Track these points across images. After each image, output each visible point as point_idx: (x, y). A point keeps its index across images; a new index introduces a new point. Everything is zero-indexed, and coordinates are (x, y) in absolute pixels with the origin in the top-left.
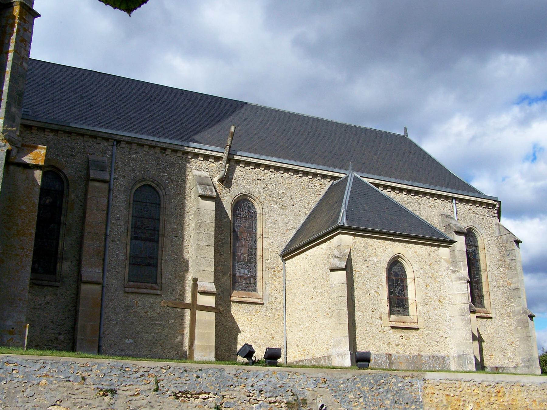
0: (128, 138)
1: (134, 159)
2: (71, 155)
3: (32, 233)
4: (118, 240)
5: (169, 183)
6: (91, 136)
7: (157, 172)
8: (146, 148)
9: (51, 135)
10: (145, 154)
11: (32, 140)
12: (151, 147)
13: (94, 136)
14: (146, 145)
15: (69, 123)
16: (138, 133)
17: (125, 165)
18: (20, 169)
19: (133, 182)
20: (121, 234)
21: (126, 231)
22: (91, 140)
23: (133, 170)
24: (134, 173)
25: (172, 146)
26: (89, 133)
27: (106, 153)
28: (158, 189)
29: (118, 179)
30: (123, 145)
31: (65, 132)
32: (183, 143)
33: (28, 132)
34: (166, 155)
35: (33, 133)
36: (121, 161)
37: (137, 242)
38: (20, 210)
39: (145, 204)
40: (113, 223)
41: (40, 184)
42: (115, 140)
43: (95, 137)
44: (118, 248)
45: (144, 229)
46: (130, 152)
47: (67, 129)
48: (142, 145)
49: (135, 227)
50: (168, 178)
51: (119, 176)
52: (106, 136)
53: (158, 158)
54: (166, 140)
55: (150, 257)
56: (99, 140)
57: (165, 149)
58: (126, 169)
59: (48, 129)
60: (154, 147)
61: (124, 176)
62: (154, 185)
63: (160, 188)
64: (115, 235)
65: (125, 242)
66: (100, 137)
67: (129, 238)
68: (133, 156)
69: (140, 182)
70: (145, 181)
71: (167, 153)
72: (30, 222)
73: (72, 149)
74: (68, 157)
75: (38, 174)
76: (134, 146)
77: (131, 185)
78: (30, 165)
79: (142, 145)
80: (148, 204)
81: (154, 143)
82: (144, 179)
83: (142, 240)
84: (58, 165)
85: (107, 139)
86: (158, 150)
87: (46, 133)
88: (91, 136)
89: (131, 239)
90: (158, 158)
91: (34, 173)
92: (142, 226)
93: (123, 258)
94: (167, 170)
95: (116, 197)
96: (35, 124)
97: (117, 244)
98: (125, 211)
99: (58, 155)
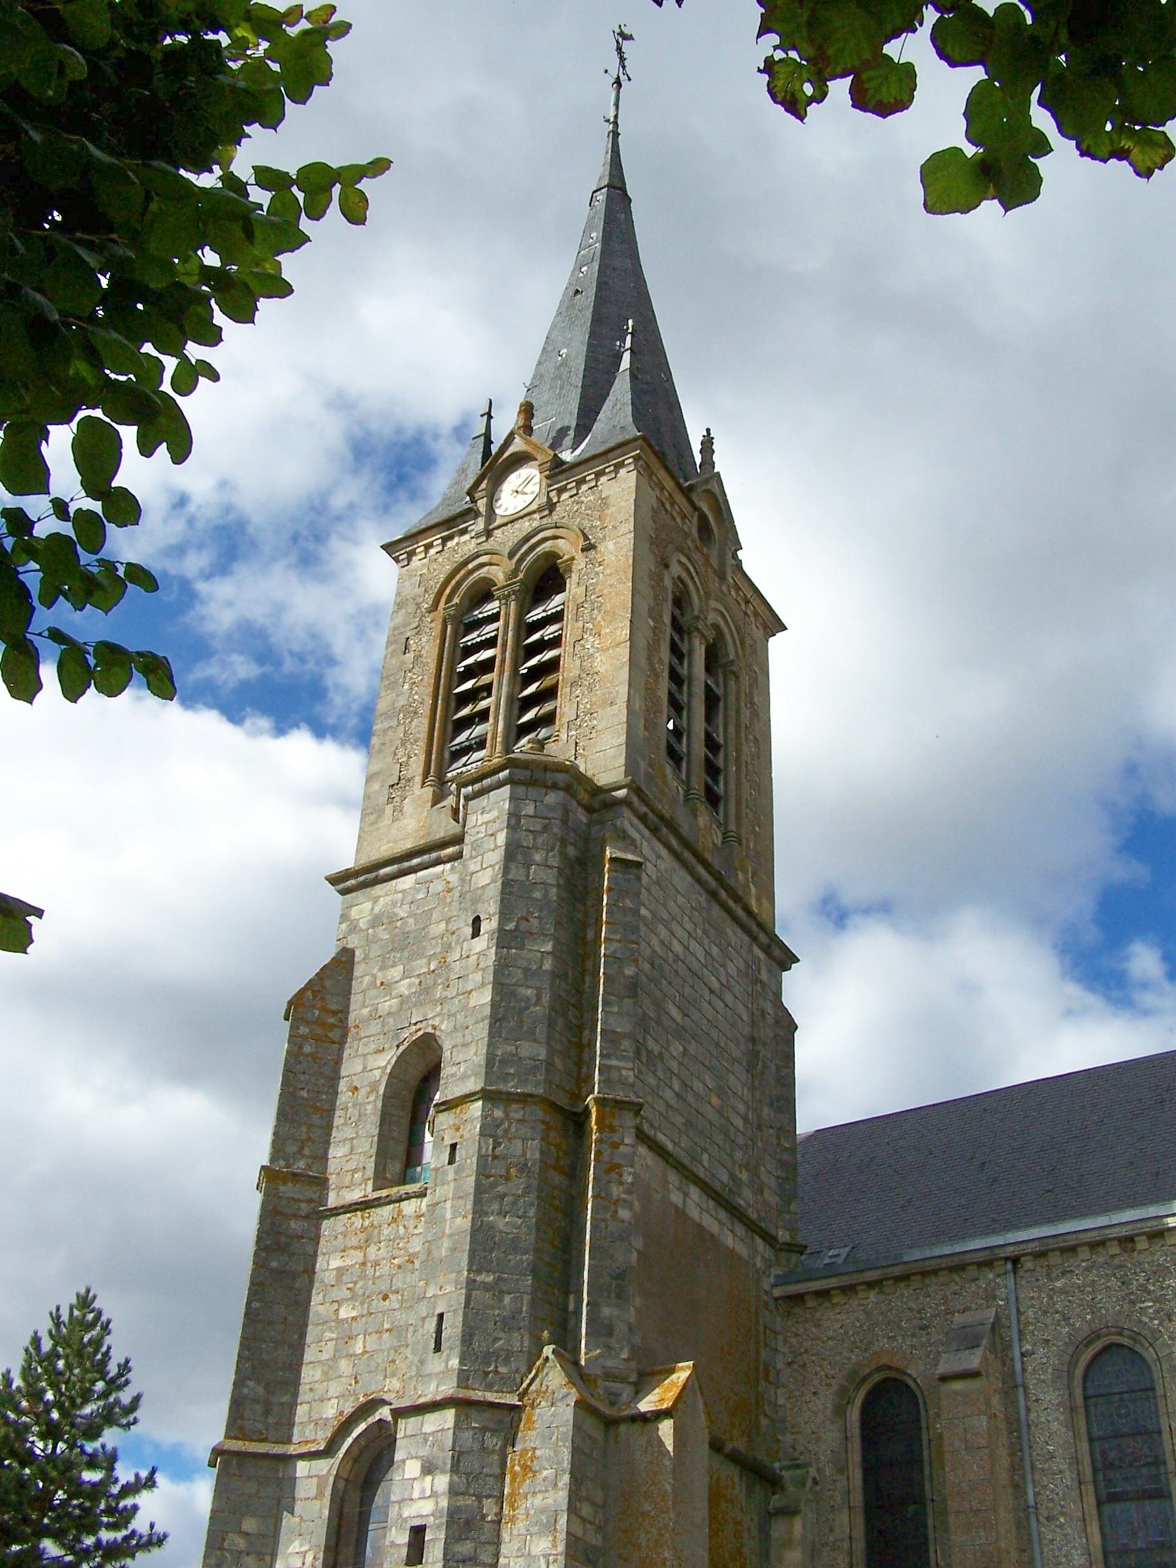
0: (1032, 1245)
1: (1063, 1291)
2: (922, 1328)
3: (665, 1559)
4: (1062, 1514)
5: (1160, 1324)
6: (952, 1269)
7: (1126, 1306)
8: (1084, 1253)
9: (873, 1296)
10: (1087, 1269)
11: (838, 1321)
12: (1096, 1245)
13: (958, 1266)
14: (969, 1264)
15: (901, 1255)
16: (1050, 1221)
17: (1045, 1313)
18: (636, 1427)
19: (1070, 1350)
20: (1064, 1495)
21: (1076, 1484)
22: (957, 1278)
23: (1066, 1318)
24: (1069, 1325)
25: (1143, 1224)
26: (944, 1263)
27: (995, 1298)
28: (1138, 1348)
29: (1033, 1353)
30: (1028, 1264)
31: (898, 1279)
32: (1152, 1211)
33: (827, 1304)
34: (1140, 1252)
35: (834, 1305)
36: (1033, 1306)
37: (1118, 1507)
38: (643, 1514)
39: (1117, 1397)
40: (1043, 1470)
41: (670, 1448)
42: (1006, 1259)
43: (962, 1268)
44: (1065, 1535)
45: (1131, 1465)
46: (1048, 1275)
47: (897, 1271)
48: (1073, 1249)
49: (1103, 1467)
50: (1157, 1311)
51: (1035, 1344)
52: (981, 1257)
53: (1120, 1267)
54: (1023, 1235)
55: (1162, 1545)
56: (971, 1271)
57: (1130, 1239)
58: (1048, 1321)
59: (859, 1284)
60: (1102, 1243)
61: (1047, 1341)
62: (1125, 1341)
63: (1142, 1345)
64: (1052, 1500)
65: (1080, 1514)
66: (972, 1264)
67: (1091, 1500)
68: (1058, 1284)
69: (1087, 1346)
70: (1099, 1337)
71: (1139, 1246)
72: (661, 1535)
73: (919, 1312)
74: (913, 1335)
75: (666, 1429)
76: (1055, 1259)
77: (1067, 1358)
78: (649, 1415)
79: (1073, 1249)
80: (1126, 1396)
81: (1095, 1233)
82: (1095, 1336)
83: (1131, 1500)
84: (896, 1363)
85: (989, 1264)
86: (1114, 1249)
87: (861, 1295)
88: (952, 1269)
89: (1099, 1504)
90: (1120, 1267)
91: (658, 1429)
92: (1120, 1460)
93: (1083, 1561)
94: (1149, 1292)
95: (1037, 1400)
96: (833, 1282)
97: (1061, 1526)
98: (1064, 1430)
99: (893, 1338)
